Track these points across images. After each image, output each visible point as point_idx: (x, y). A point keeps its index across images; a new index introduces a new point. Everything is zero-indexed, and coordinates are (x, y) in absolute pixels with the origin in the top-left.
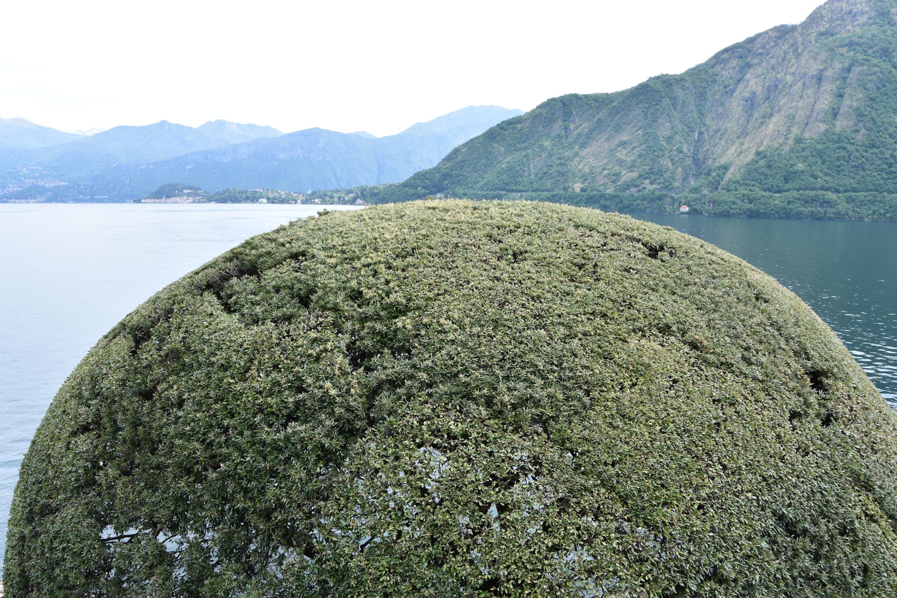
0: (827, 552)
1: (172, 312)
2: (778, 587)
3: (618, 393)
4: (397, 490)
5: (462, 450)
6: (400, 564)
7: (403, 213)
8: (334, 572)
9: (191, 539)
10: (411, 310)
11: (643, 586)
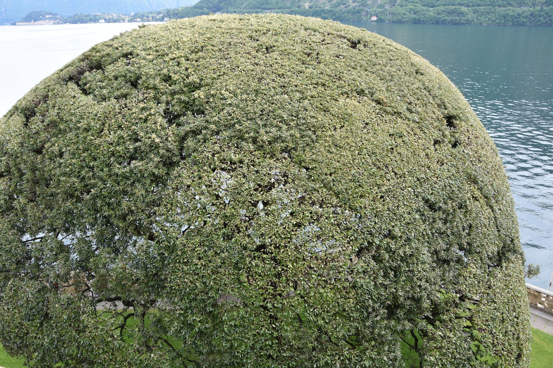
0: (451, 218)
1: (48, 97)
2: (424, 239)
3: (333, 132)
4: (201, 197)
5: (240, 171)
6: (207, 240)
7: (194, 24)
8: (167, 248)
9: (78, 236)
10: (203, 86)
11: (349, 243)
